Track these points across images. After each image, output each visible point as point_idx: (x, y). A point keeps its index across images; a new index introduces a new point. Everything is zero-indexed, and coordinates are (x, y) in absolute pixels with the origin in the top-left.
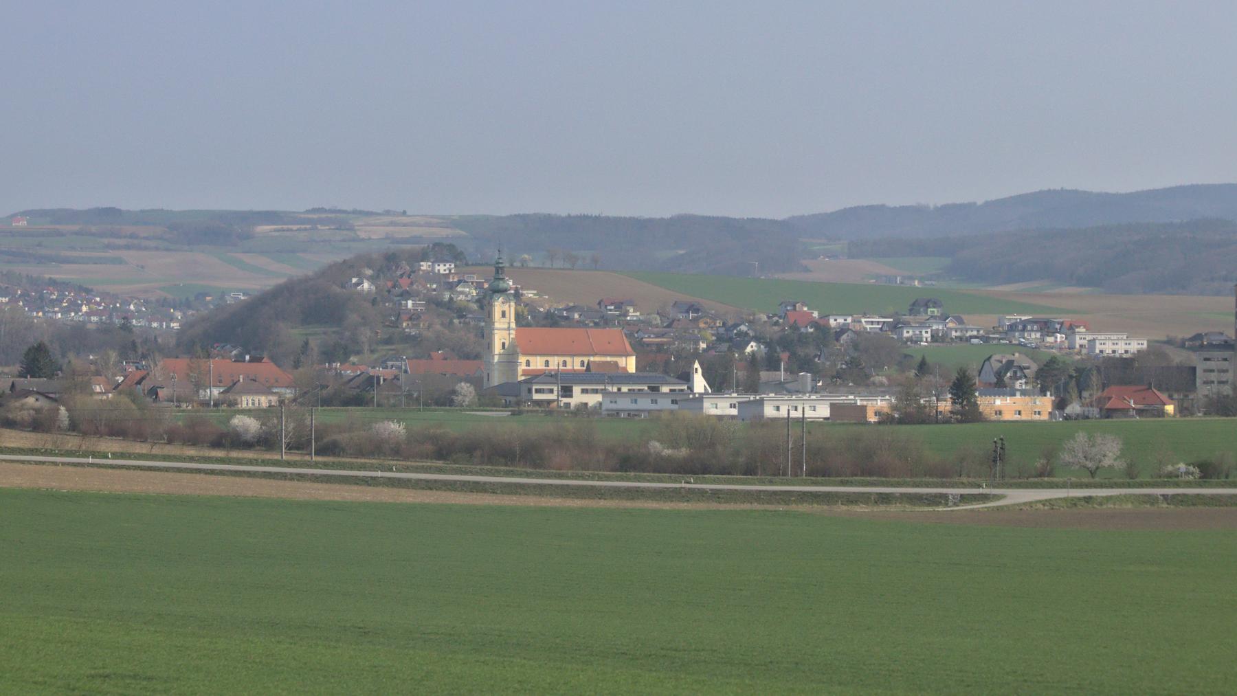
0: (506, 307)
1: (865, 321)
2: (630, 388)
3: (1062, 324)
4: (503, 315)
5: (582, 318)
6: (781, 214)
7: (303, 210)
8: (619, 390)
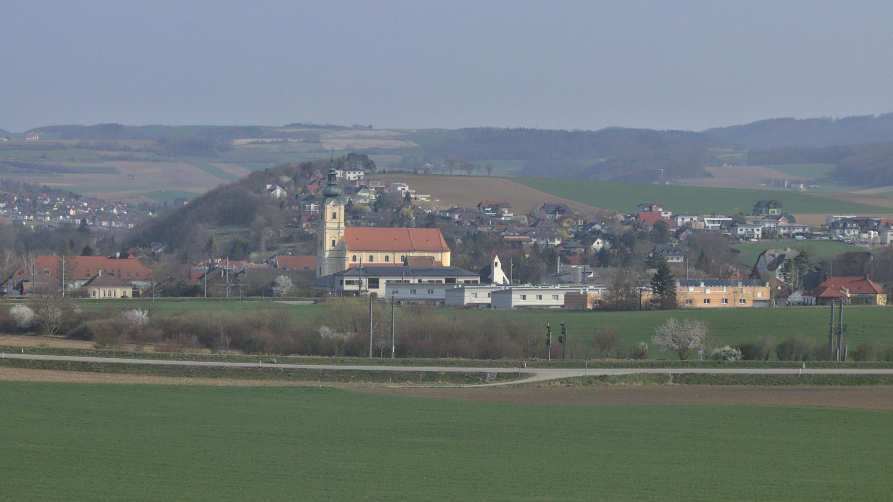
0: (336, 210)
1: (708, 221)
2: (388, 279)
3: (879, 222)
4: (334, 216)
5: (461, 218)
6: (699, 127)
7: (282, 125)
8: (420, 281)
